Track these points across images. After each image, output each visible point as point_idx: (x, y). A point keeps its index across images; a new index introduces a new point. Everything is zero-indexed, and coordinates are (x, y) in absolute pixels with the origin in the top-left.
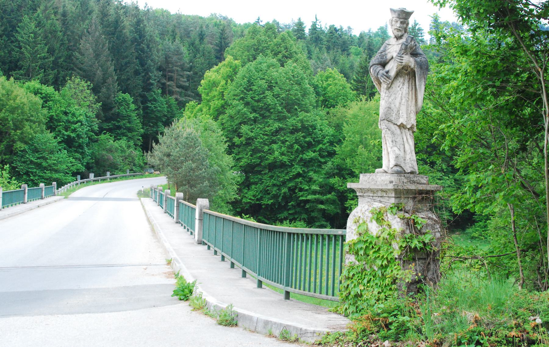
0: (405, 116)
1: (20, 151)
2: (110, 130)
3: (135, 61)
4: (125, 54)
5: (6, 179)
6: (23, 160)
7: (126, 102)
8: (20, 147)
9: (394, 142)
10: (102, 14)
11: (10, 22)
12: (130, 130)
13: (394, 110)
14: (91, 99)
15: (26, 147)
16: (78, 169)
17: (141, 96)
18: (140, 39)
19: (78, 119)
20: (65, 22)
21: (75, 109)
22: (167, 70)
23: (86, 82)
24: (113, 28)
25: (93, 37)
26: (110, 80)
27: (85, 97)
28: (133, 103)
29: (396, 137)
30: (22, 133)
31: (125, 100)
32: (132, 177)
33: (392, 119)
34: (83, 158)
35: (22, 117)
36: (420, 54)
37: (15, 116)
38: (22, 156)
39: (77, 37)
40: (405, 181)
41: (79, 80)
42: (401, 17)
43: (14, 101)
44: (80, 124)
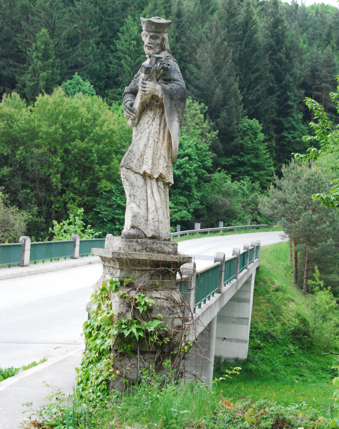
0: (150, 162)
1: (105, 191)
2: (228, 168)
3: (268, 75)
4: (256, 66)
5: (79, 227)
6: (108, 203)
7: (253, 130)
8: (106, 187)
9: (132, 197)
10: (228, 12)
11: (111, 26)
12: (257, 167)
13: (136, 155)
14: (205, 125)
15: (113, 187)
16: (182, 218)
17: (273, 121)
18: (277, 46)
19: (186, 151)
20: (179, 25)
21: (183, 139)
22: (314, 87)
23: (200, 103)
24: (241, 32)
25: (213, 44)
26: (232, 102)
27: (197, 124)
28: (262, 131)
29: (135, 190)
30: (109, 169)
31: (251, 128)
32: (255, 230)
33: (133, 166)
34: (190, 203)
35: (109, 148)
36: (175, 80)
37: (101, 146)
38: (108, 199)
39: (194, 45)
40: (138, 248)
41: (191, 100)
42: (150, 30)
43: (101, 128)
44: (187, 158)
